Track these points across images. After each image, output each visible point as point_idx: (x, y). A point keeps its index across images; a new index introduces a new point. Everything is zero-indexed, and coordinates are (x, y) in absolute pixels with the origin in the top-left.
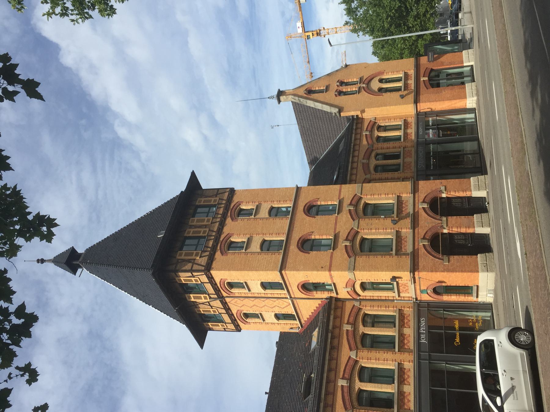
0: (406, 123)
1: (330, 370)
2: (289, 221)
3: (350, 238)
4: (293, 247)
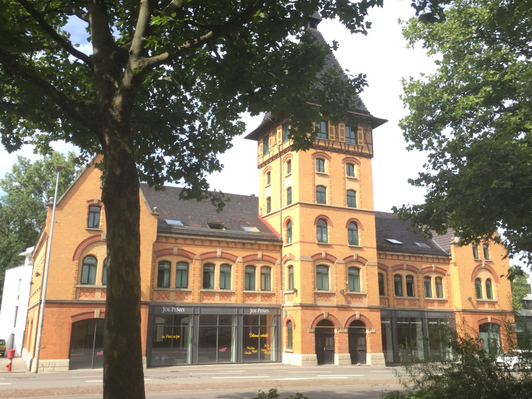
0: (443, 302)
1: (227, 243)
2: (343, 207)
3: (328, 257)
4: (319, 212)
